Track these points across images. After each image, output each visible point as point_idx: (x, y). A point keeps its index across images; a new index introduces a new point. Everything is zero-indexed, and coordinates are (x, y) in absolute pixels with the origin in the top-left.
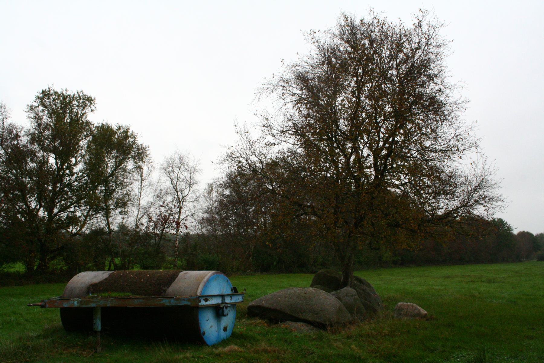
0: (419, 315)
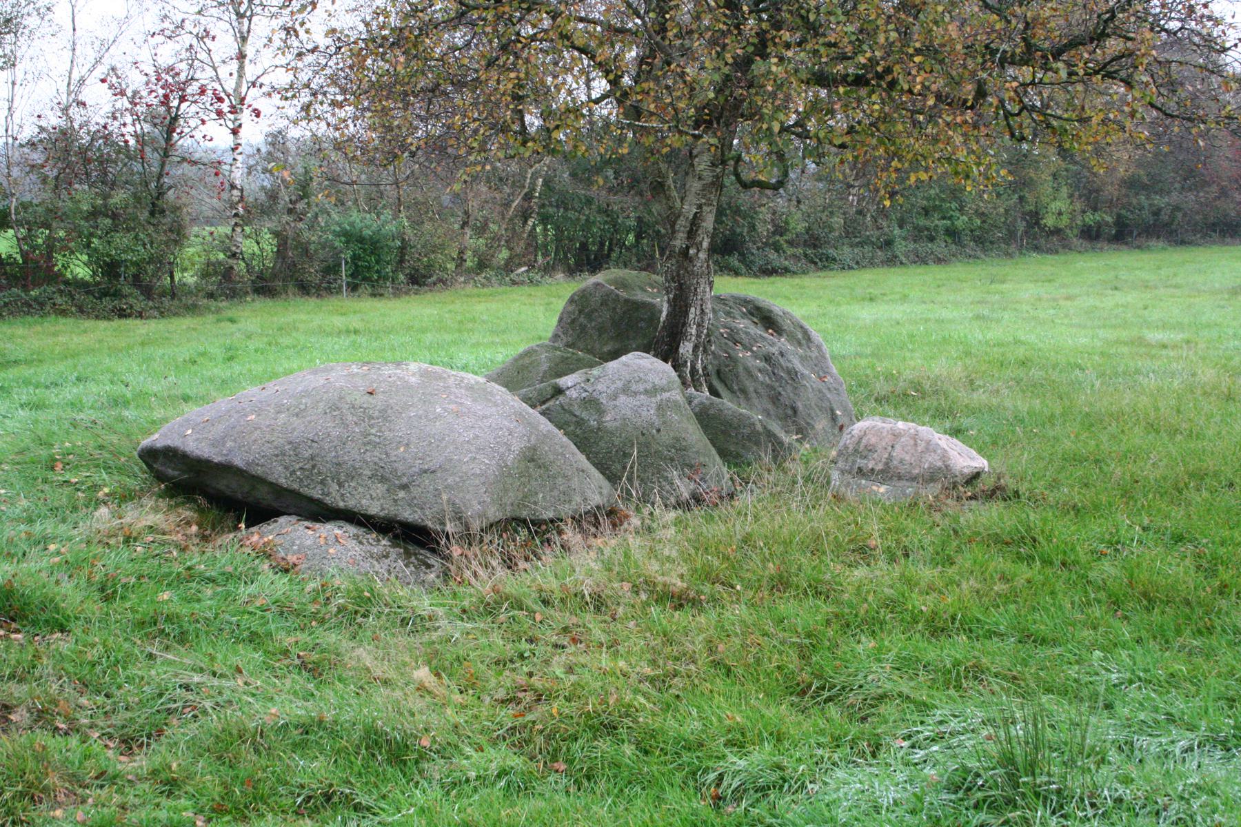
0: (940, 475)
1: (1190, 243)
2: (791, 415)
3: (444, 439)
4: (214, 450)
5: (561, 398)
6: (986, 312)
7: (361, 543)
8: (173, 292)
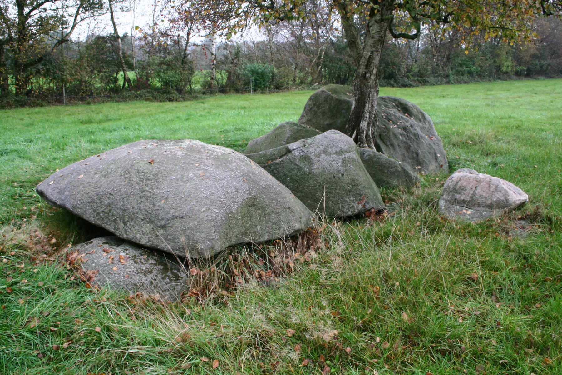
1: (553, 77)
2: (417, 160)
3: (190, 195)
4: (59, 196)
5: (290, 155)
6: (490, 103)
7: (136, 262)
8: (191, 92)
